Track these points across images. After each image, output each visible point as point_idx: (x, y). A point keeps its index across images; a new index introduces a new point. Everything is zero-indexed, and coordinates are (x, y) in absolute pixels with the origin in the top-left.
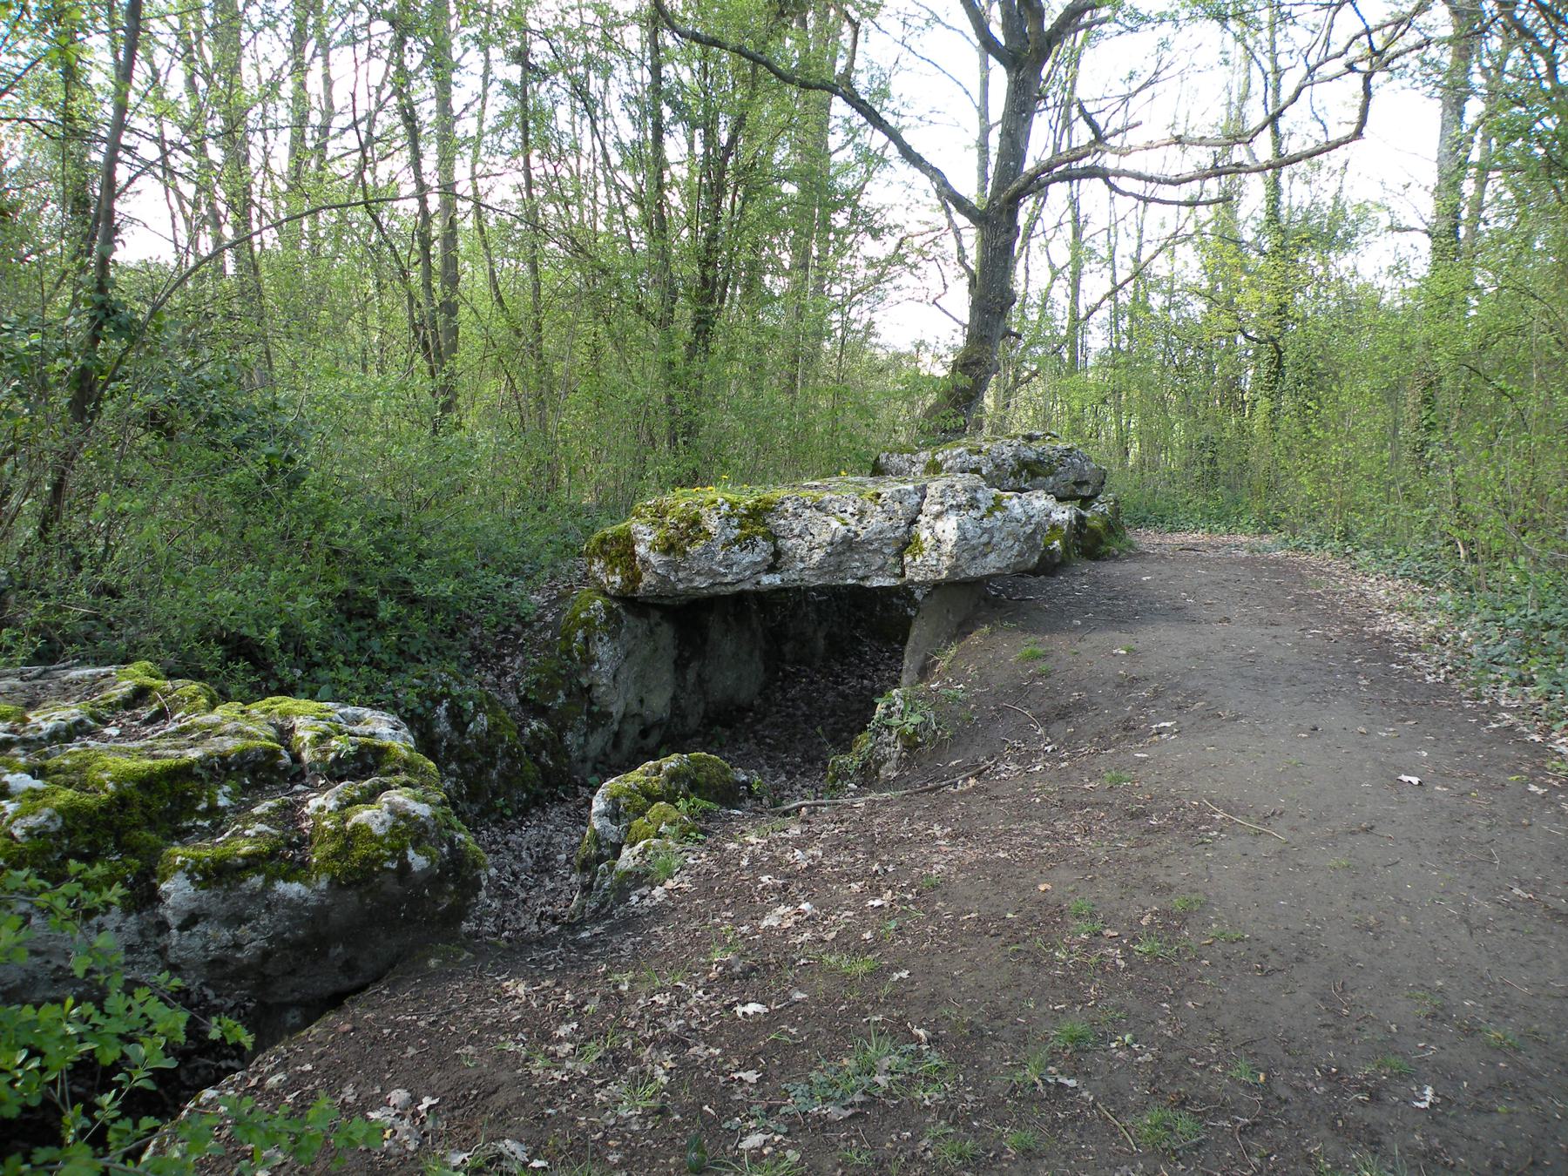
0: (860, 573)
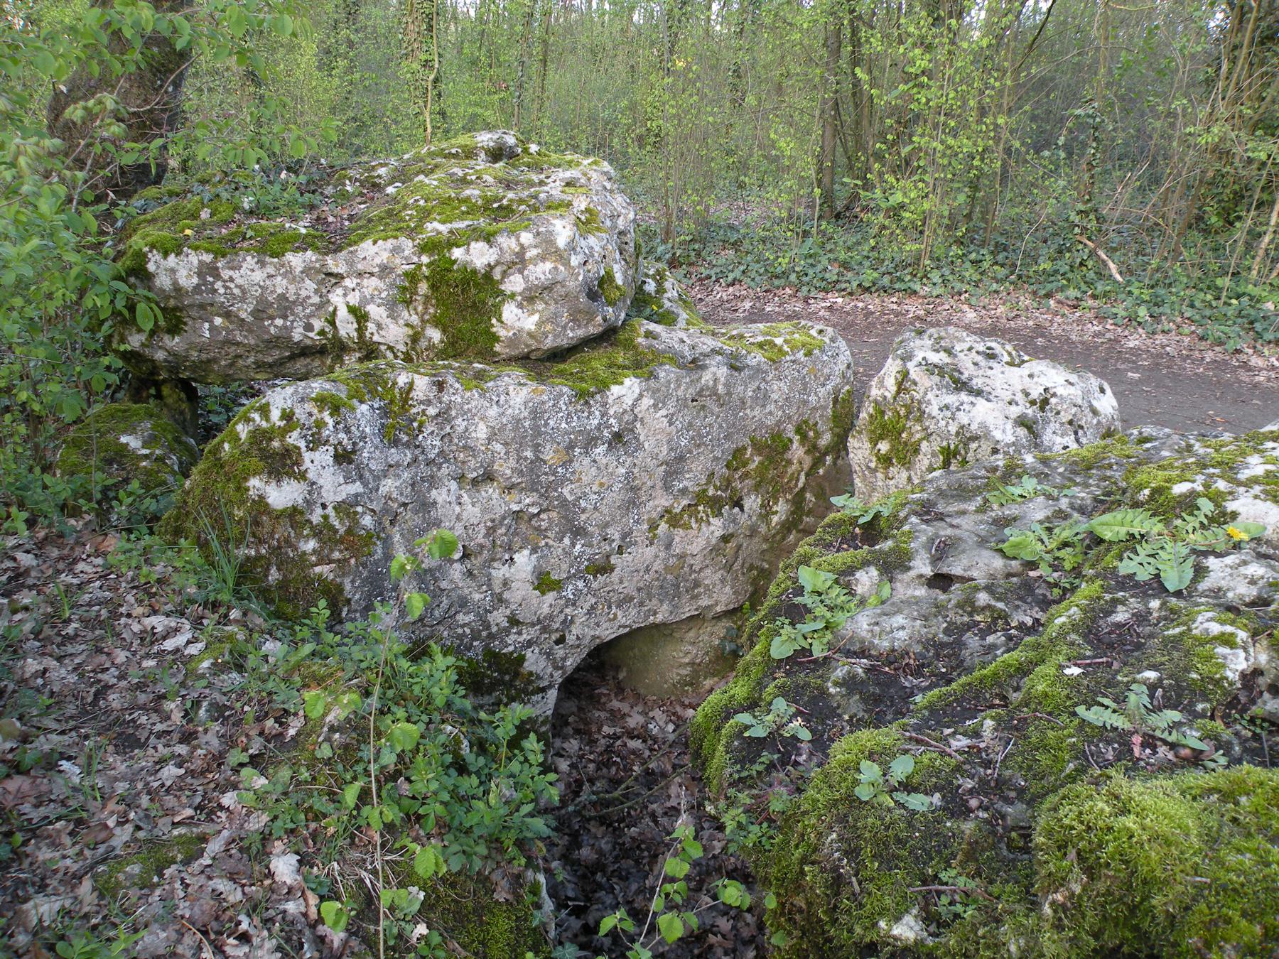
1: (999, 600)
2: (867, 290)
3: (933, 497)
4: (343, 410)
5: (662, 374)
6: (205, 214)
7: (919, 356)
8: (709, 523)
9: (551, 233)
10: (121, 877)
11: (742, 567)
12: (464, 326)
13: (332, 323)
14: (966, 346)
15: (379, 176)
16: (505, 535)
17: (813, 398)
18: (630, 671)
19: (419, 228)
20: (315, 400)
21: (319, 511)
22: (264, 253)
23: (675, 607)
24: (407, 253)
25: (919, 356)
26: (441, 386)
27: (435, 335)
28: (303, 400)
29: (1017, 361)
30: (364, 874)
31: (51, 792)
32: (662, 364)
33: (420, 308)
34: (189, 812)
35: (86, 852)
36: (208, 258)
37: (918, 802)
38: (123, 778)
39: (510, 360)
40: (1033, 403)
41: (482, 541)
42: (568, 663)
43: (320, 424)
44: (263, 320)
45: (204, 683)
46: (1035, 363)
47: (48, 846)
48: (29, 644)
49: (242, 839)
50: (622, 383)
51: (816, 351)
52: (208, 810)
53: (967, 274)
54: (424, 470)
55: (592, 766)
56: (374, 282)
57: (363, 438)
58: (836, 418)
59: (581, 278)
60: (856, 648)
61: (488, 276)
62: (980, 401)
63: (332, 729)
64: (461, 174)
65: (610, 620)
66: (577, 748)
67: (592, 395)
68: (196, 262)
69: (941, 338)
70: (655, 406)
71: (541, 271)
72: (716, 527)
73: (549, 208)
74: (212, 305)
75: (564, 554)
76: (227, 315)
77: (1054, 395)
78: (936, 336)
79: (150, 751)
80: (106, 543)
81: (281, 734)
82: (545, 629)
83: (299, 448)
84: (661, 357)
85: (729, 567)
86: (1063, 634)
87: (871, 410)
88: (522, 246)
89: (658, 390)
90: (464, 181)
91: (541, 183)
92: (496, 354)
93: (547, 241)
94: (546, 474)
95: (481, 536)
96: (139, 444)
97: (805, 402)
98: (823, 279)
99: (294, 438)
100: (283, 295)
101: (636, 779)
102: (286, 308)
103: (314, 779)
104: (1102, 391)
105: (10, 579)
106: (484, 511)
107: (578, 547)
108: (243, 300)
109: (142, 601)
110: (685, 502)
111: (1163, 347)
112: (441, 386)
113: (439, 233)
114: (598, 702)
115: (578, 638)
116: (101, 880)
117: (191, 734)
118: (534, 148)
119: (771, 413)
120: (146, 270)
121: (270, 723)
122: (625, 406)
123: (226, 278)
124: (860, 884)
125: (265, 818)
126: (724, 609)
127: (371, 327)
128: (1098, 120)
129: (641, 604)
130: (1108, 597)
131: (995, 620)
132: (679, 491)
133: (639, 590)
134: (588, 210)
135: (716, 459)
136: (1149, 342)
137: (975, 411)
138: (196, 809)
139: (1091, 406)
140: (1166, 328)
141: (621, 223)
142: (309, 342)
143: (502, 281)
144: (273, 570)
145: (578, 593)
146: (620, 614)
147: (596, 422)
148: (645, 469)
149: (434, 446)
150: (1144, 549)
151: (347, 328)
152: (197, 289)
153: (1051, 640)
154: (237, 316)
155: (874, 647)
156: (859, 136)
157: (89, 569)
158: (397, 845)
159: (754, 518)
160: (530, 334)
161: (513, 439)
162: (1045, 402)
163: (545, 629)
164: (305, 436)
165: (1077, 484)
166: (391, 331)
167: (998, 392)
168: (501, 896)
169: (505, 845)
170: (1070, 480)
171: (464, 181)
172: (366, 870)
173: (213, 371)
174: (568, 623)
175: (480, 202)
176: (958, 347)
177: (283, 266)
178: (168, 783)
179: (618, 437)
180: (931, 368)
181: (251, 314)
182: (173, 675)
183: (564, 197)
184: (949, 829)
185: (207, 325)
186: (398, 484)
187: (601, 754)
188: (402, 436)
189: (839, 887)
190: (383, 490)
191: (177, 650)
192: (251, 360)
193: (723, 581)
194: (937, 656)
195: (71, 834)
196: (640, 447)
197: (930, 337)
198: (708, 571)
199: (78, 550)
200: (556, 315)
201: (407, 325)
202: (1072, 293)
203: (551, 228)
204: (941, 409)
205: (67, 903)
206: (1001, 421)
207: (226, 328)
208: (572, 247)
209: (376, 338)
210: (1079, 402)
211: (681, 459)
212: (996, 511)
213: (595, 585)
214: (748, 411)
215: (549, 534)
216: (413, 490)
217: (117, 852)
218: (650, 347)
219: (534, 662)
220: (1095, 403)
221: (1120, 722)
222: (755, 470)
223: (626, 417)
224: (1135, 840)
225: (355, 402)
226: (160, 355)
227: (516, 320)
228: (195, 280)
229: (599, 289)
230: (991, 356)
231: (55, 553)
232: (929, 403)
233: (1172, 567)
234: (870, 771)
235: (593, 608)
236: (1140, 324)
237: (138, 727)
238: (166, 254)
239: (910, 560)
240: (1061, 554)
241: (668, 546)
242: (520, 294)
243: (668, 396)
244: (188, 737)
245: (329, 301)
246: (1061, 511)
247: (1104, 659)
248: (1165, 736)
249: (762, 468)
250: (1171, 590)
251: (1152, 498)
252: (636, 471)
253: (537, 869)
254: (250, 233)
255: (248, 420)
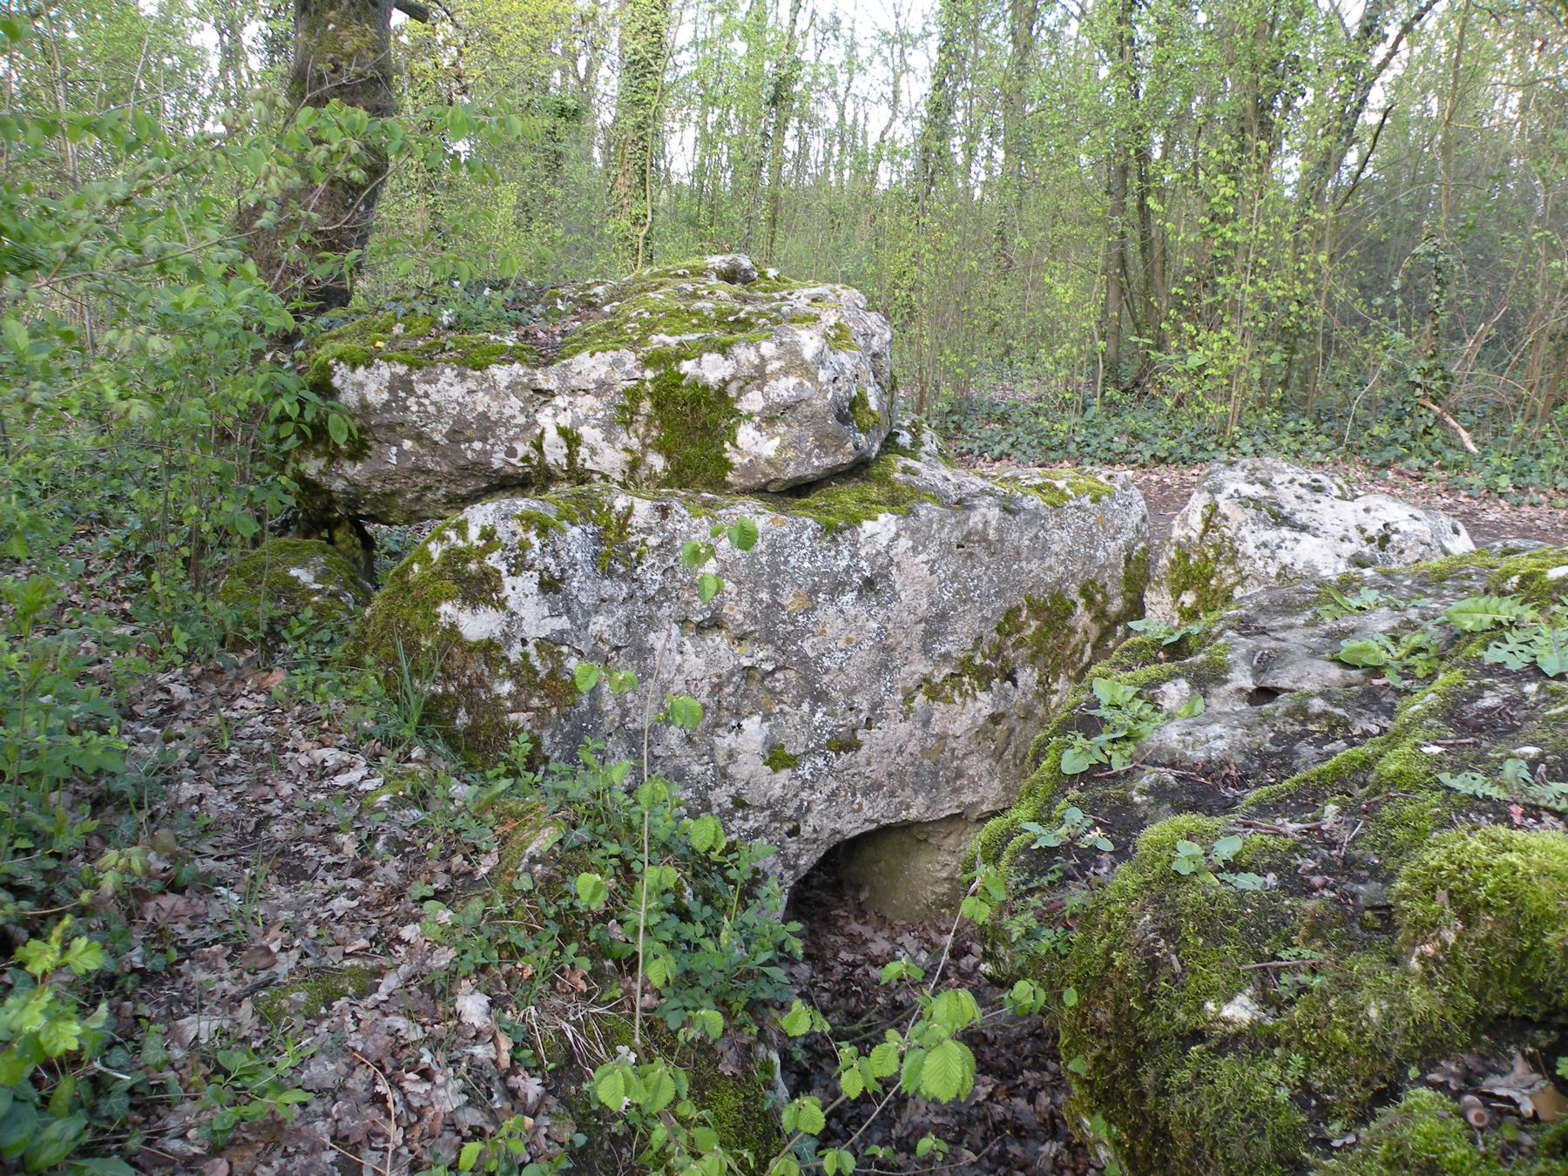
1: (1336, 706)
2: (1163, 460)
3: (1251, 613)
4: (551, 531)
5: (923, 512)
6: (398, 329)
7: (1230, 488)
8: (975, 698)
9: (797, 343)
10: (285, 1003)
11: (1015, 757)
12: (690, 450)
13: (539, 447)
14: (1287, 478)
15: (596, 295)
16: (733, 695)
17: (1100, 554)
18: (874, 890)
19: (643, 341)
20: (521, 518)
21: (518, 647)
22: (466, 365)
23: (933, 801)
24: (628, 367)
25: (1230, 488)
26: (664, 512)
27: (657, 462)
28: (506, 517)
29: (1349, 496)
30: (565, 1025)
31: (207, 914)
32: (923, 501)
33: (641, 430)
34: (363, 943)
35: (246, 975)
36: (401, 370)
37: (1248, 881)
38: (288, 907)
39: (745, 491)
40: (1370, 540)
41: (705, 700)
42: (802, 862)
43: (525, 546)
44: (459, 442)
45: (382, 816)
46: (1370, 497)
47: (204, 969)
48: (184, 771)
49: (423, 976)
50: (876, 519)
51: (1105, 498)
52: (387, 942)
53: (1284, 442)
54: (642, 609)
55: (826, 996)
56: (589, 400)
57: (573, 565)
58: (1128, 579)
59: (829, 396)
60: (1166, 760)
61: (722, 393)
62: (1306, 537)
63: (533, 860)
64: (690, 288)
65: (854, 811)
66: (807, 974)
67: (841, 531)
68: (387, 375)
69: (1256, 469)
70: (914, 549)
71: (784, 387)
72: (984, 704)
73: (793, 321)
74: (402, 425)
75: (802, 724)
76: (419, 437)
77: (1396, 531)
78: (1250, 467)
79: (319, 883)
80: (270, 679)
81: (470, 873)
82: (775, 817)
83: (499, 572)
84: (919, 494)
85: (998, 756)
86: (1417, 721)
87: (1173, 555)
88: (762, 358)
89: (918, 530)
90: (694, 296)
91: (783, 299)
92: (728, 485)
93: (792, 353)
94: (784, 622)
95: (704, 694)
96: (311, 578)
97: (1092, 558)
98: (1109, 450)
99: (494, 560)
100: (484, 414)
101: (879, 1013)
102: (487, 429)
103: (511, 913)
104: (1456, 531)
105: (162, 712)
106: (710, 663)
107: (819, 715)
108: (438, 420)
109: (310, 736)
110: (947, 671)
111: (1532, 520)
112: (664, 512)
113: (665, 345)
114: (835, 925)
115: (815, 831)
116: (263, 1006)
117: (365, 868)
118: (772, 272)
119: (1050, 568)
120: (330, 385)
121: (458, 860)
122: (879, 547)
123: (421, 393)
124: (1181, 962)
125: (452, 953)
126: (992, 808)
127: (583, 452)
128: (1441, 258)
129: (892, 794)
130: (1472, 683)
131: (1332, 729)
132: (941, 655)
133: (890, 775)
134: (837, 326)
135: (985, 619)
136: (1513, 515)
137: (1298, 548)
138: (371, 940)
139: (1442, 546)
140: (1535, 500)
141: (875, 344)
142: (510, 470)
143: (738, 399)
144: (462, 712)
145: (816, 773)
146: (866, 804)
147: (844, 563)
148: (900, 625)
149: (654, 581)
150: (1513, 638)
151: (555, 453)
152: (386, 406)
153: (1403, 726)
154: (430, 439)
155: (1187, 758)
156: (1147, 286)
157: (250, 705)
158: (605, 997)
159: (1030, 696)
160: (769, 461)
161: (747, 576)
162: (1385, 539)
163: (775, 817)
164: (507, 558)
165: (1428, 596)
166: (606, 456)
167: (1328, 527)
168: (727, 1069)
169: (734, 1008)
170: (1419, 591)
171: (694, 296)
172: (567, 1021)
173: (397, 506)
174: (804, 810)
175: (713, 315)
176: (1277, 479)
177: (485, 380)
178: (339, 914)
179: (869, 583)
180: (1244, 502)
181: (446, 436)
182: (346, 809)
183: (810, 310)
184: (1289, 907)
185: (394, 450)
186: (610, 622)
187: (837, 982)
188: (617, 566)
189: (1155, 970)
190: (593, 629)
191: (350, 786)
192: (443, 491)
193: (991, 773)
194: (1264, 766)
195: (229, 958)
196: (895, 597)
197: (1243, 468)
198: (973, 759)
199: (237, 688)
200: (800, 439)
201: (625, 449)
202: (1414, 462)
203: (796, 338)
204: (1257, 547)
205: (226, 1024)
206: (1331, 559)
207: (416, 453)
208: (820, 361)
209: (588, 465)
210: (1428, 539)
211: (943, 617)
212: (1329, 624)
213: (837, 764)
214: (1024, 564)
215: (785, 698)
216: (628, 631)
217: (281, 980)
218: (908, 483)
220: (1447, 545)
221: (1495, 793)
222: (1031, 637)
223: (880, 560)
224: (1519, 874)
225: (566, 524)
226: (339, 485)
227: (753, 445)
228: (385, 396)
229: (850, 411)
230: (1317, 489)
231: (212, 689)
232: (1243, 540)
233: (1551, 652)
234: (1188, 849)
235: (834, 793)
236: (1501, 495)
237: (304, 859)
238: (354, 367)
239: (1226, 672)
240: (1412, 660)
241: (926, 723)
242: (759, 414)
243: (930, 538)
244: (361, 872)
245: (536, 422)
246: (1409, 621)
247: (1471, 740)
248: (1552, 804)
249: (1040, 636)
251: (1522, 585)
252: (890, 626)
253: (769, 1044)
254: (450, 344)
255: (442, 538)
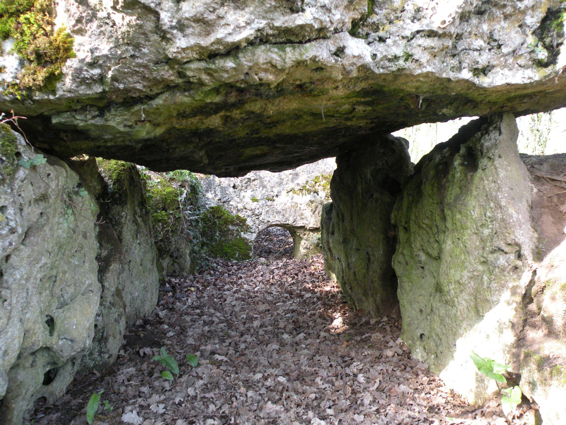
0: (483, 59)
219: (249, 222)
241: (292, 199)
250: (522, 150)
